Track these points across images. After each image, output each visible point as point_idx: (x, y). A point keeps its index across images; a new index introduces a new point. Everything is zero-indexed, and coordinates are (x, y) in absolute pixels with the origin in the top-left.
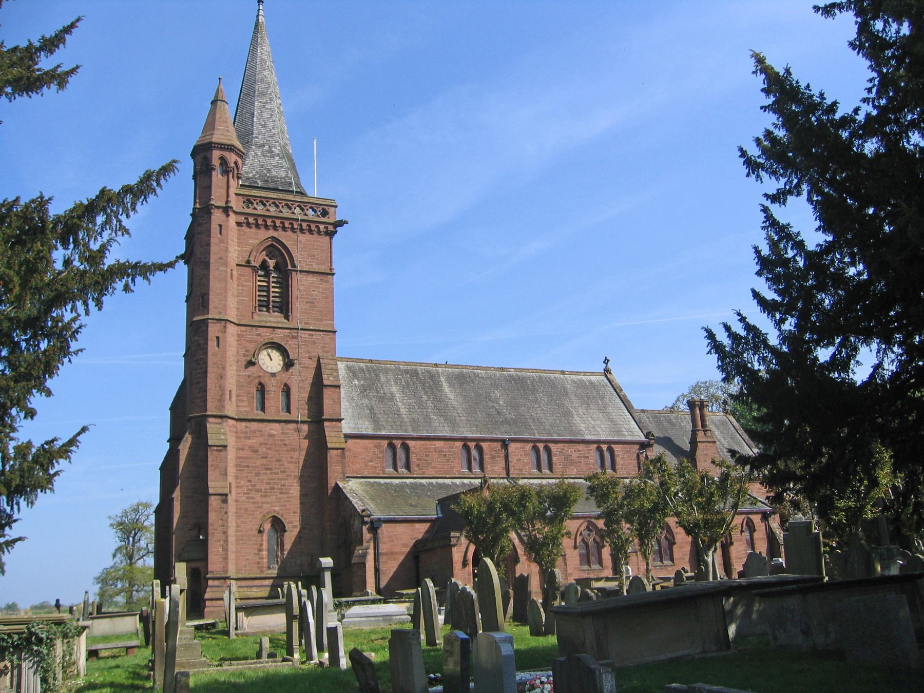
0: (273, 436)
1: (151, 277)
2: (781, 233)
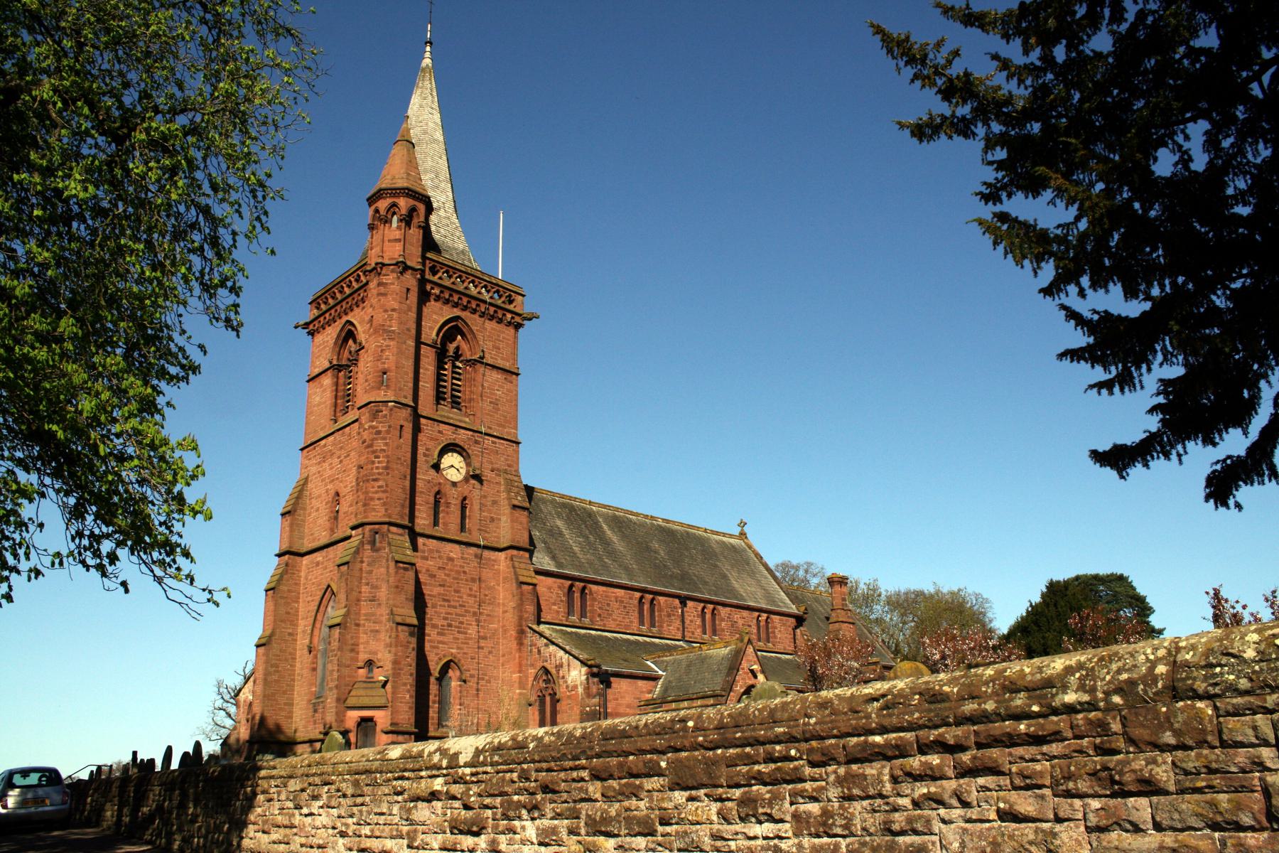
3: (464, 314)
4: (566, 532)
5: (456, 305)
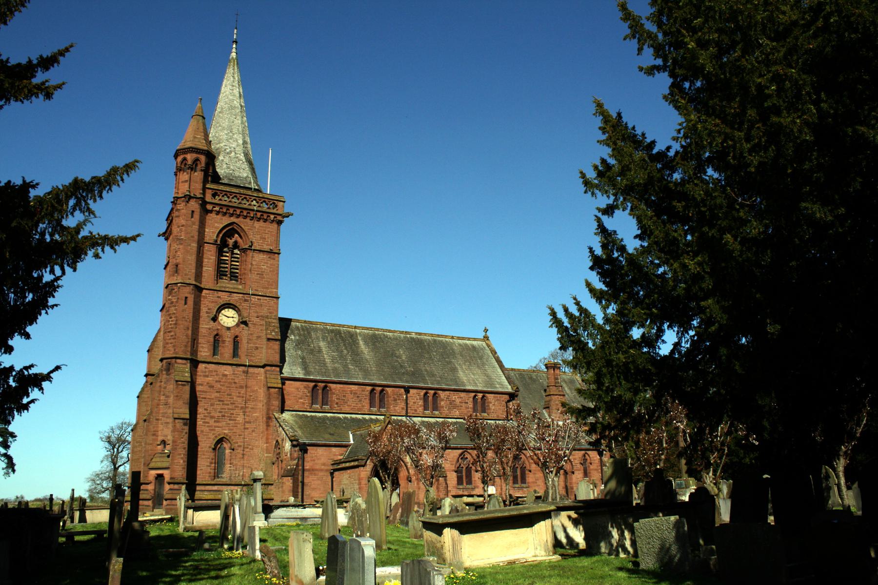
0: (226, 375)
1: (117, 247)
2: (607, 236)
3: (233, 219)
4: (324, 350)
5: (232, 215)
